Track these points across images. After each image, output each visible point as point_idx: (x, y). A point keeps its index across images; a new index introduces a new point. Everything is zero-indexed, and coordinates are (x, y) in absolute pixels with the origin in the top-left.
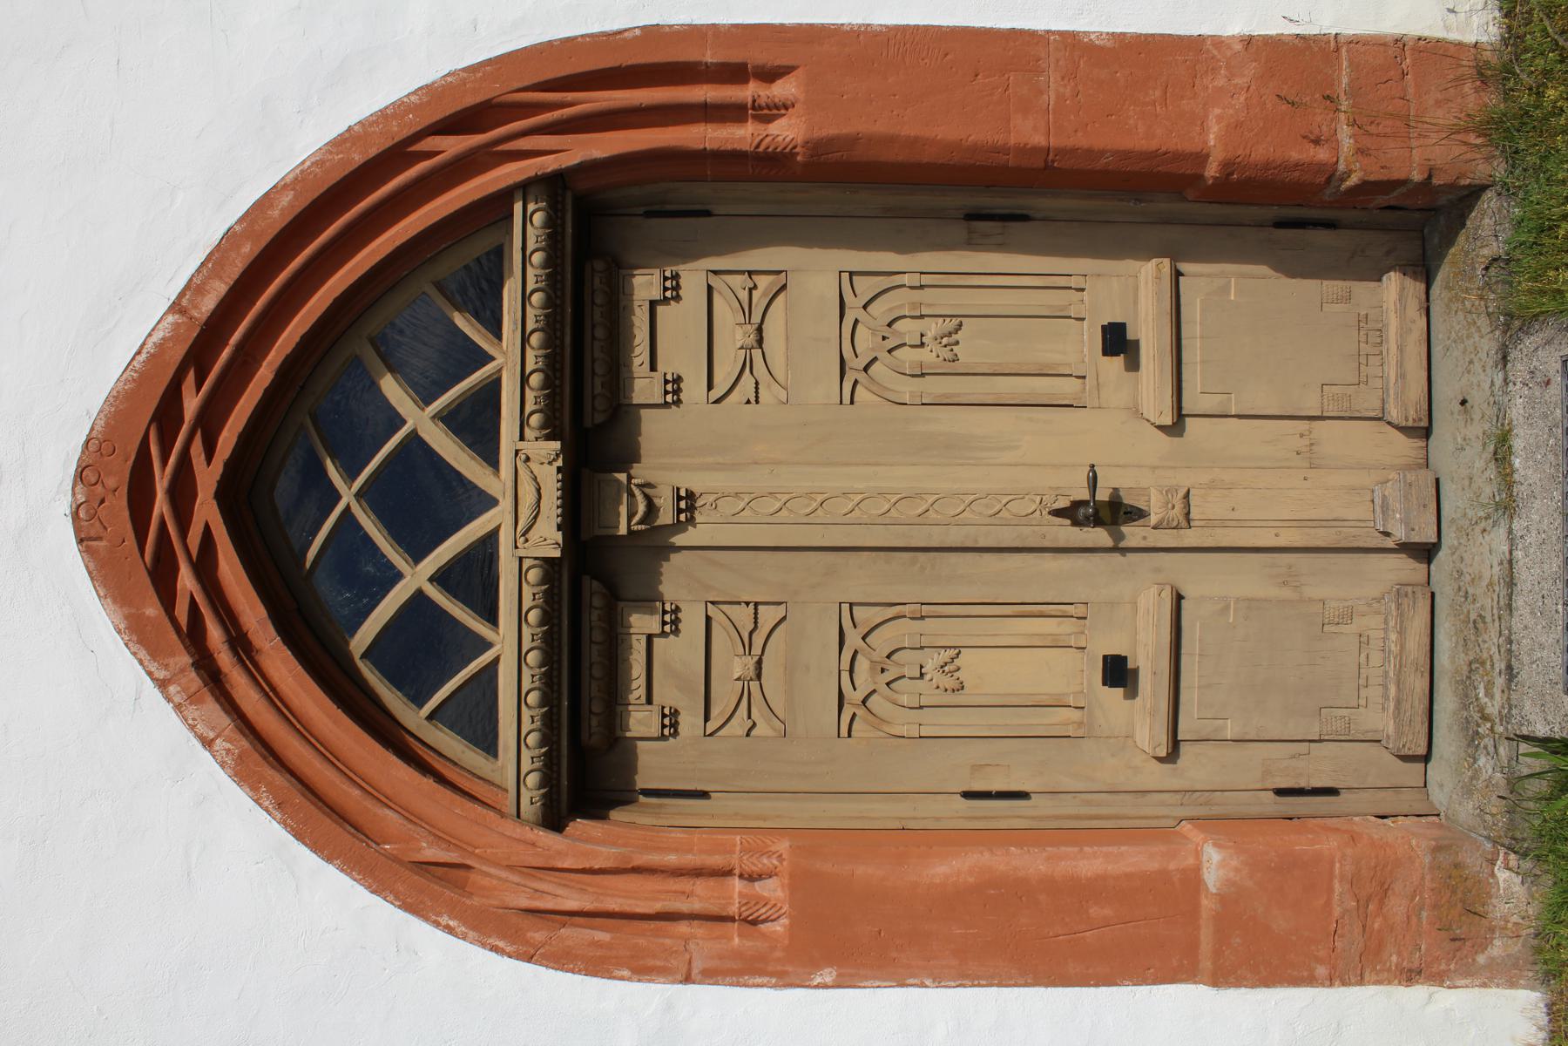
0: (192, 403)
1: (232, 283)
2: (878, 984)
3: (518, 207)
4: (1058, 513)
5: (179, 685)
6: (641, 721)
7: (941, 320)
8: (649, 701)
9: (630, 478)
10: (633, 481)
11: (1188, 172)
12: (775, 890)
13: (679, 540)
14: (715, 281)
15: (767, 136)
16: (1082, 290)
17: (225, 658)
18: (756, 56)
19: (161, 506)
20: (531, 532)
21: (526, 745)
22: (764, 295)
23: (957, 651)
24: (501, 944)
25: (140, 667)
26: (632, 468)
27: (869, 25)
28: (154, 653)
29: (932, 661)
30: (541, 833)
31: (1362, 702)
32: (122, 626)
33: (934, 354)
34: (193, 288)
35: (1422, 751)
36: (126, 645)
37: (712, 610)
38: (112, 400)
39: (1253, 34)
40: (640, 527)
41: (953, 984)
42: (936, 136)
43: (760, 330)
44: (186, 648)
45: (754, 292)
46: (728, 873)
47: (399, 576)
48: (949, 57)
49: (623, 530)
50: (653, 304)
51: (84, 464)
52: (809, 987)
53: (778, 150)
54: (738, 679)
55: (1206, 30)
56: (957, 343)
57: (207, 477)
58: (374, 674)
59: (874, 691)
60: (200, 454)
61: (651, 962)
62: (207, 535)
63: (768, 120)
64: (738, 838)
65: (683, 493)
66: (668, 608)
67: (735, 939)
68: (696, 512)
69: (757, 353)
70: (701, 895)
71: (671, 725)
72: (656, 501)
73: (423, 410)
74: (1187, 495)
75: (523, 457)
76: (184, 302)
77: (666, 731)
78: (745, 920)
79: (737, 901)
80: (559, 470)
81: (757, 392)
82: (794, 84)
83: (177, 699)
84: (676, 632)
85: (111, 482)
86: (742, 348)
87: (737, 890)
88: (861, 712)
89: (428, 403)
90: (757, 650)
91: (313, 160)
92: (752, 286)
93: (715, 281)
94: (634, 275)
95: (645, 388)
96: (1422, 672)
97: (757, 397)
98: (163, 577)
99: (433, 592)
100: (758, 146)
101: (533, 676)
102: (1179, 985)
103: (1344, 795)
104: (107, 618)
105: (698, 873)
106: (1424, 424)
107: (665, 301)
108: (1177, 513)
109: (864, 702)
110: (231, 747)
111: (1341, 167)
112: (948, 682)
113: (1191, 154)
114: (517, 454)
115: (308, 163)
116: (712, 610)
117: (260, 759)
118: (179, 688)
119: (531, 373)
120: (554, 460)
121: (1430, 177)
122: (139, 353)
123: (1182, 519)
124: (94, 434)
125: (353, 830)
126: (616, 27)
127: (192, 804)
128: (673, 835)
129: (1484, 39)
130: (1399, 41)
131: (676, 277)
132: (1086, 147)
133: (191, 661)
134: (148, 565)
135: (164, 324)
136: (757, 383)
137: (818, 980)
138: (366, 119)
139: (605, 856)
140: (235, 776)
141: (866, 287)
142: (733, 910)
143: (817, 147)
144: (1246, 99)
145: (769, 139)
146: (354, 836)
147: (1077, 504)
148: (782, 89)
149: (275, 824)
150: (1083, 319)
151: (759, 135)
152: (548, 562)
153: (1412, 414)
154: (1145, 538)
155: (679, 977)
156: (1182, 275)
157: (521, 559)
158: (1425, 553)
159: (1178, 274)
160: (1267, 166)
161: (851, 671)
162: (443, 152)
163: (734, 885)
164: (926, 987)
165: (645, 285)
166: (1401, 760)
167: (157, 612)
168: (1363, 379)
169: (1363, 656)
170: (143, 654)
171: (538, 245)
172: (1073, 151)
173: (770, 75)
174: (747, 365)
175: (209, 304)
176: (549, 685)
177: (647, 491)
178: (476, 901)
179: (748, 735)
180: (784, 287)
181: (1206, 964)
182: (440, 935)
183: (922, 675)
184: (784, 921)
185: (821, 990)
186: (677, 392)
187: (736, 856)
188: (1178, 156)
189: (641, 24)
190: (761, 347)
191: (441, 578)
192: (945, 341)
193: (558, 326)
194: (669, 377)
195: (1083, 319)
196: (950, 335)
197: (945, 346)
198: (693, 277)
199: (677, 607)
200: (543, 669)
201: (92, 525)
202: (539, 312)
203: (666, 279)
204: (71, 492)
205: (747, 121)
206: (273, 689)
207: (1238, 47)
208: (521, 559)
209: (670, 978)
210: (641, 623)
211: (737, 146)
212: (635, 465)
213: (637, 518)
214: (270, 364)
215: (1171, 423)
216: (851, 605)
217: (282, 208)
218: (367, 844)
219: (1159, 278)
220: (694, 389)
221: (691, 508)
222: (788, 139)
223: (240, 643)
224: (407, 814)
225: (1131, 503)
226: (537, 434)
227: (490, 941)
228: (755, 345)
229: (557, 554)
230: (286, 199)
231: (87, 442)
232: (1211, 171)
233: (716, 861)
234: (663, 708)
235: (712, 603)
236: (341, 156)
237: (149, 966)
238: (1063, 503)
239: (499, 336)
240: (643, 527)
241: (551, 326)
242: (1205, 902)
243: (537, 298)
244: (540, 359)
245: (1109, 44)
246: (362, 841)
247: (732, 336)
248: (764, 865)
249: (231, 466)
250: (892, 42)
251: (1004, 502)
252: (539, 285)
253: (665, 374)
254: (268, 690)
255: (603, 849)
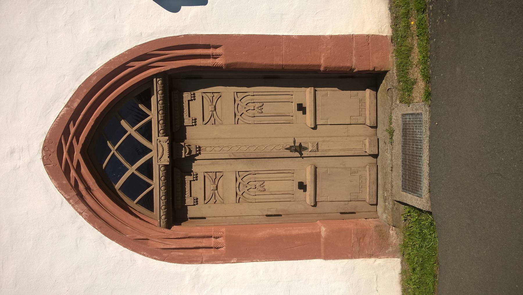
0: (72, 130)
1: (81, 99)
2: (246, 261)
3: (155, 80)
4: (287, 149)
5: (73, 200)
6: (189, 201)
7: (259, 103)
8: (191, 196)
9: (185, 144)
10: (186, 145)
11: (317, 69)
12: (222, 241)
13: (196, 158)
14: (204, 95)
15: (216, 62)
16: (293, 95)
17: (84, 192)
18: (212, 43)
19: (65, 155)
20: (161, 159)
21: (162, 209)
22: (216, 98)
23: (264, 182)
24: (157, 257)
25: (62, 196)
26: (184, 141)
27: (239, 34)
28: (66, 193)
29: (258, 184)
30: (166, 230)
31: (361, 192)
32: (57, 186)
33: (257, 112)
34: (71, 101)
35: (375, 203)
36: (58, 191)
37: (206, 174)
38: (51, 129)
39: (332, 35)
40: (187, 155)
41: (264, 261)
42: (256, 62)
43: (215, 107)
44: (74, 191)
45: (213, 97)
46: (211, 237)
47: (127, 169)
48: (259, 42)
49: (183, 156)
50: (189, 101)
51: (45, 146)
52: (230, 263)
53: (216, 66)
54: (212, 190)
55: (321, 34)
56: (262, 109)
57: (77, 148)
58: (122, 193)
59: (244, 192)
60: (75, 143)
61: (193, 259)
62: (78, 163)
63: (216, 58)
64: (213, 228)
65: (198, 147)
66: (195, 174)
67: (213, 252)
68: (201, 151)
69: (214, 112)
70: (205, 242)
71: (196, 202)
72: (191, 149)
73: (132, 129)
74: (318, 144)
75: (159, 141)
76: (69, 105)
77: (195, 179)
78: (215, 248)
79: (213, 243)
80: (168, 144)
81: (215, 122)
82: (222, 49)
83: (72, 203)
84: (197, 180)
85: (52, 150)
86: (211, 111)
87: (213, 241)
88: (241, 197)
89: (133, 127)
90: (216, 183)
91: (101, 68)
92: (213, 96)
93: (204, 95)
94: (183, 94)
95: (187, 121)
96: (375, 184)
97: (215, 123)
98: (67, 172)
99: (137, 173)
100: (213, 65)
101: (163, 193)
102: (317, 259)
103: (357, 214)
104: (53, 184)
105: (204, 237)
106: (375, 125)
107: (192, 100)
108: (315, 148)
109: (242, 194)
110: (87, 214)
111: (353, 67)
112: (262, 189)
113: (317, 65)
114: (157, 140)
115: (100, 69)
116: (206, 174)
117: (95, 217)
118: (73, 201)
119: (160, 121)
120: (167, 141)
121: (374, 69)
122: (57, 117)
123: (316, 150)
124: (47, 138)
125: (119, 232)
126: (177, 35)
127: (77, 229)
128: (197, 228)
129: (388, 35)
130: (368, 36)
131: (194, 94)
132: (292, 64)
133: (76, 194)
134: (63, 171)
135: (64, 110)
136: (215, 120)
137: (233, 261)
138: (115, 58)
139: (182, 234)
140: (88, 221)
141: (240, 95)
142: (212, 245)
143: (228, 65)
144: (330, 51)
145: (216, 63)
146: (119, 234)
147: (291, 147)
148: (218, 51)
149: (99, 232)
150: (293, 102)
151: (214, 62)
152: (165, 166)
153: (372, 123)
154: (307, 154)
155: (200, 262)
156: (317, 91)
157: (159, 165)
158: (375, 156)
159: (315, 91)
160: (335, 68)
161: (239, 187)
162: (135, 66)
163: (212, 240)
164: (258, 262)
165: (187, 96)
166: (371, 205)
167: (66, 182)
168: (361, 114)
169: (361, 181)
170: (63, 193)
171: (160, 89)
172: (288, 65)
173: (216, 47)
174: (212, 115)
175: (76, 105)
176: (167, 195)
177: (190, 147)
178: (150, 248)
179: (215, 203)
180: (221, 96)
181: (323, 254)
182: (141, 256)
183: (256, 188)
184: (224, 247)
185: (233, 264)
186: (195, 122)
187: (213, 233)
188: (314, 66)
189: (184, 34)
190: (216, 111)
191: (138, 169)
192: (260, 108)
193: (166, 108)
194: (193, 119)
195: (293, 102)
196: (261, 107)
197: (260, 109)
198: (198, 93)
199: (197, 174)
200: (165, 191)
201: (48, 161)
202: (161, 105)
203: (192, 95)
204: (41, 153)
205: (211, 58)
206: (97, 199)
207: (329, 38)
208: (159, 165)
209: (198, 263)
210: (188, 178)
211: (208, 65)
212: (185, 140)
213: (187, 153)
214: (93, 119)
215: (313, 127)
216: (238, 172)
217: (94, 81)
218: (123, 236)
219: (310, 92)
220: (199, 121)
221: (200, 150)
222: (221, 63)
223: (88, 189)
224: (132, 227)
225: (304, 146)
226: (162, 135)
227: (154, 257)
228: (214, 110)
229: (168, 163)
230: (95, 78)
231: (45, 140)
232: (322, 69)
233: (208, 234)
234: (194, 198)
235: (205, 172)
236: (108, 67)
237: (68, 269)
238: (288, 146)
239: (151, 110)
240: (188, 155)
241: (165, 109)
242: (322, 240)
243: (160, 102)
244: (162, 117)
245: (298, 38)
246: (122, 235)
247: (208, 108)
248: (219, 234)
249: (83, 145)
250: (245, 39)
251: (274, 147)
252: (161, 99)
253: (192, 118)
254: (96, 200)
255: (181, 233)
